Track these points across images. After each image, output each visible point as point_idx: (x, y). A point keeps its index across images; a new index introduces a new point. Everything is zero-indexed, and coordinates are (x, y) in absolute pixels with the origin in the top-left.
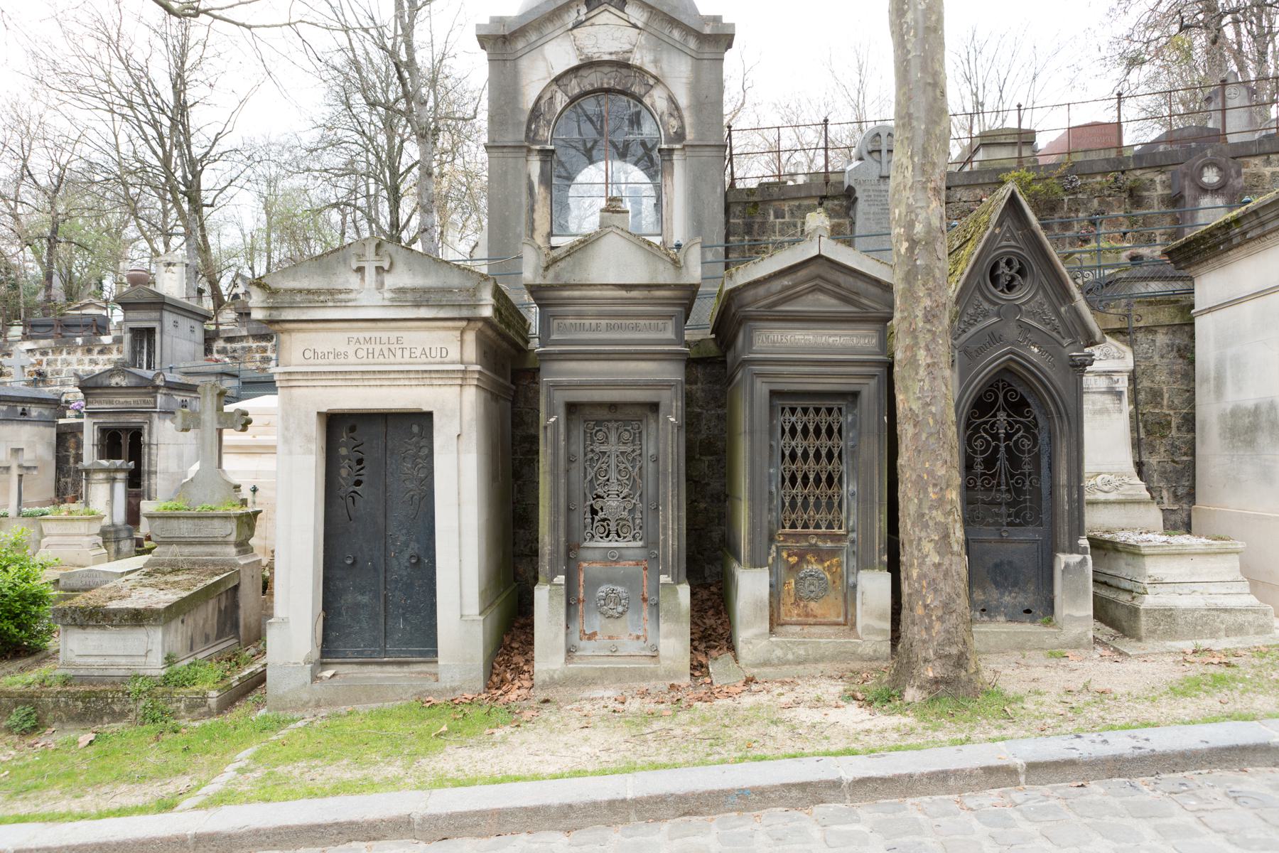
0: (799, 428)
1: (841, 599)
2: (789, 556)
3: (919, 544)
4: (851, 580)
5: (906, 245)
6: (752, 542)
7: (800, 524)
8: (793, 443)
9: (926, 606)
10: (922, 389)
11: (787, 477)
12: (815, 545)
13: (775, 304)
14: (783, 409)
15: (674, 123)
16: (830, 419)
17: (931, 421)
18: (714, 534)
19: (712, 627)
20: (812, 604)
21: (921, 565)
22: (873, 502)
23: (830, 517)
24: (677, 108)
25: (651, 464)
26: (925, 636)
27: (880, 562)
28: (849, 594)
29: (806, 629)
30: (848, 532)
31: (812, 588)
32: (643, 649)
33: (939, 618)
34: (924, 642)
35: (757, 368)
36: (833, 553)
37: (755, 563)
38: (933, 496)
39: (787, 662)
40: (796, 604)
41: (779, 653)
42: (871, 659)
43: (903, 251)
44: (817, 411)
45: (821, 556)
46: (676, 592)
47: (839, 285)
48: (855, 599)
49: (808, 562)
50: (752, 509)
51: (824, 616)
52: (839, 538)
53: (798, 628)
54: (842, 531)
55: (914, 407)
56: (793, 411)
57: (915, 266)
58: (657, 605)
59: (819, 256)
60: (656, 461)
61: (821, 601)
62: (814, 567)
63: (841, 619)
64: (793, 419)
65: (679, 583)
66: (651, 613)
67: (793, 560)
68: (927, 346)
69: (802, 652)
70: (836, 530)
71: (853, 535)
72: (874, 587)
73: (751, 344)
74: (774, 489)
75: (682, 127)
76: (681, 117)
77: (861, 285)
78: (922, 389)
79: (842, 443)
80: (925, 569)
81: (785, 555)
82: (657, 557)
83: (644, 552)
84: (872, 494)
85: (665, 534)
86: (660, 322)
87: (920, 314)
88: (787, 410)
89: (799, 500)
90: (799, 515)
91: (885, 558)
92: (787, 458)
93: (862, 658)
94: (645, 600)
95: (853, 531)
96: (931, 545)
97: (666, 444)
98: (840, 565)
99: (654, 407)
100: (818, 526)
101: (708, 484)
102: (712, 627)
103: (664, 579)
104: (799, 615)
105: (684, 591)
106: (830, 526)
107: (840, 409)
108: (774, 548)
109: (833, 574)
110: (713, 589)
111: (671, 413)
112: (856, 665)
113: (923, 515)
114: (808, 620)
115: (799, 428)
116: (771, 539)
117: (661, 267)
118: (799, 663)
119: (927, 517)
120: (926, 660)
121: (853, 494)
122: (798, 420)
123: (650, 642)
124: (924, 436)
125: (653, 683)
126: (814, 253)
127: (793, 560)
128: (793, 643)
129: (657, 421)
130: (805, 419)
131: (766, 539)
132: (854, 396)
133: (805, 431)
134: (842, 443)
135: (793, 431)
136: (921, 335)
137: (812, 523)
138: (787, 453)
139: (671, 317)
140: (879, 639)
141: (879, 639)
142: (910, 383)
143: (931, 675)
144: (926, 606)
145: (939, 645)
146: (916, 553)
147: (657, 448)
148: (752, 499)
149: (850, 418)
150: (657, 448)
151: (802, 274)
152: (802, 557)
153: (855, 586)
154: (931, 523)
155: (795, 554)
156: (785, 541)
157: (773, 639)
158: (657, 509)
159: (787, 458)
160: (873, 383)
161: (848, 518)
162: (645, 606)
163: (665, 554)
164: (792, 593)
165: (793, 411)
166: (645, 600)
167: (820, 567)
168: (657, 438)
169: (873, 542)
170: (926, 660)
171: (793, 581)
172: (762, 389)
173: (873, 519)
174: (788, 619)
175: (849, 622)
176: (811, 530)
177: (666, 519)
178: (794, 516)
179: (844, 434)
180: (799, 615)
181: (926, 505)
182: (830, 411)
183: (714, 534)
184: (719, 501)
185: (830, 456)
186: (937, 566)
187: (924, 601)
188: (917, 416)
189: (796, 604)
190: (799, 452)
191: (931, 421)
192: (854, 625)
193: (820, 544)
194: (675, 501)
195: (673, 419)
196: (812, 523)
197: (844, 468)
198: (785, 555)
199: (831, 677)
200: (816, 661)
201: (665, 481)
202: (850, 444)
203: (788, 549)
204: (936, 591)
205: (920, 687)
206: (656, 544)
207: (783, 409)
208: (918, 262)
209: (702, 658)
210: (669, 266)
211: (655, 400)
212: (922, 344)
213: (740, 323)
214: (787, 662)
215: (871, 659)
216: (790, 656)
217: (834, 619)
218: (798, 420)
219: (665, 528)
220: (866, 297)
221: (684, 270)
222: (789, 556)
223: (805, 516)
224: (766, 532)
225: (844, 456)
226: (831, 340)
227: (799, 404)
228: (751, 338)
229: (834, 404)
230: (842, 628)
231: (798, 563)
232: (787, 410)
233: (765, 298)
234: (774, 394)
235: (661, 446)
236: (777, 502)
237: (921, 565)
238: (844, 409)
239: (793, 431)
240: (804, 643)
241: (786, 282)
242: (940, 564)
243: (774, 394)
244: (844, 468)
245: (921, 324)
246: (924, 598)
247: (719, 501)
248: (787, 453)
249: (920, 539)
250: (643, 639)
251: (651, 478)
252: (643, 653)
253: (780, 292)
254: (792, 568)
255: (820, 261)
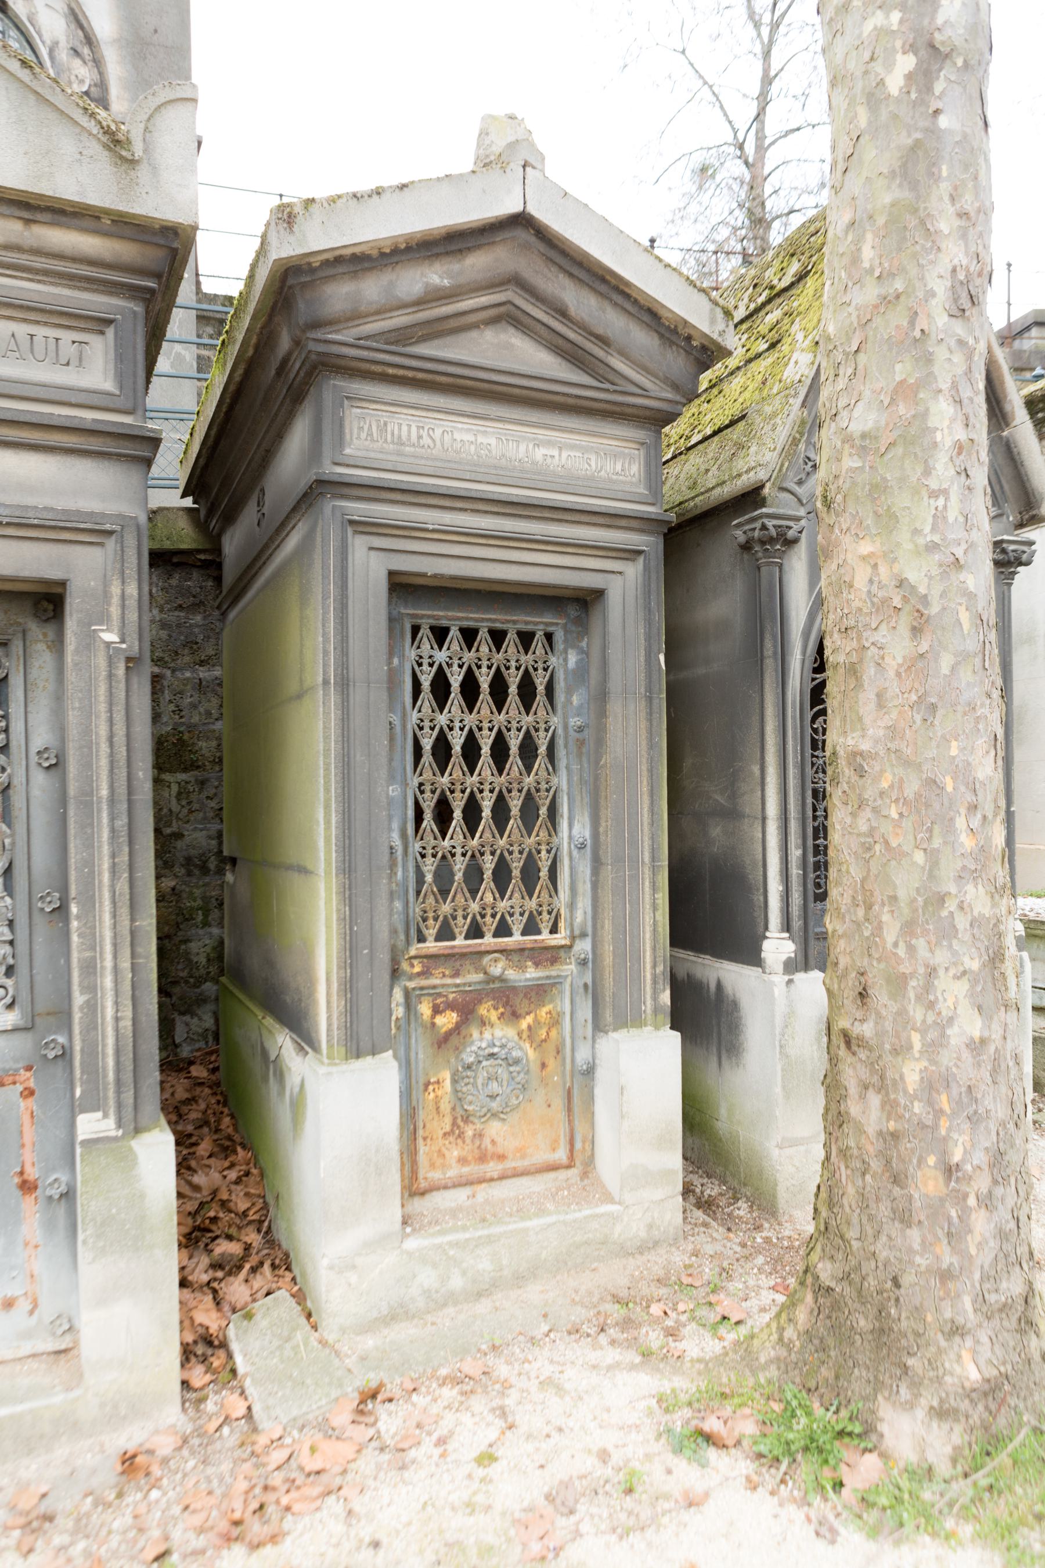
0: (456, 680)
1: (559, 1102)
2: (436, 1011)
3: (928, 987)
4: (583, 1055)
5: (907, 63)
6: (349, 987)
7: (461, 926)
8: (442, 719)
9: (950, 1171)
10: (939, 518)
11: (429, 806)
12: (501, 979)
13: (402, 336)
14: (415, 630)
15: (82, 74)
16: (527, 660)
17: (964, 617)
18: (194, 946)
19: (232, 1225)
20: (495, 1129)
21: (932, 1048)
22: (635, 862)
23: (532, 904)
24: (89, 40)
25: (39, 778)
26: (948, 1259)
27: (656, 1010)
28: (579, 1090)
29: (483, 1192)
30: (573, 938)
31: (494, 1087)
32: (27, 1335)
33: (987, 1202)
34: (946, 1276)
35: (358, 509)
36: (540, 992)
37: (358, 1045)
38: (967, 842)
39: (451, 1299)
40: (455, 1132)
41: (427, 1278)
42: (641, 1250)
43: (895, 83)
44: (498, 637)
45: (511, 1001)
46: (129, 1160)
47: (562, 313)
48: (590, 1099)
49: (483, 1023)
50: (349, 895)
51: (521, 1151)
52: (550, 955)
53: (461, 1195)
54: (560, 939)
55: (913, 576)
56: (440, 635)
57: (933, 131)
58: (68, 1196)
59: (522, 221)
60: (56, 766)
61: (514, 1118)
62: (495, 1033)
63: (561, 1155)
64: (441, 656)
65: (137, 1131)
66: (49, 1226)
67: (447, 1020)
68: (955, 386)
69: (485, 1265)
70: (545, 937)
71: (584, 946)
72: (646, 1063)
73: (340, 441)
74: (397, 842)
75: (102, 84)
76: (98, 63)
77: (612, 321)
78: (939, 518)
79: (555, 720)
80: (946, 1058)
81: (425, 1009)
82: (65, 1055)
83: (23, 1043)
84: (634, 843)
85: (91, 988)
86: (67, 336)
87: (941, 288)
88: (425, 631)
89: (459, 865)
90: (461, 906)
91: (666, 997)
92: (427, 758)
93: (625, 1252)
94: (27, 1187)
95: (583, 935)
96: (962, 988)
97: (88, 712)
98: (555, 1021)
99: (47, 601)
100: (503, 930)
101: (178, 836)
102: (232, 1225)
103: (90, 1125)
104: (462, 1161)
105: (157, 1150)
106: (532, 928)
107: (549, 637)
108: (398, 995)
109: (540, 1045)
110: (198, 1071)
111: (103, 618)
112: (616, 1275)
113: (941, 899)
114: (487, 1167)
115: (456, 680)
116: (395, 973)
117: (67, 144)
118: (480, 1295)
119: (951, 905)
120: (956, 1330)
121: (582, 847)
122: (453, 658)
123: (47, 1311)
124: (946, 662)
125: (61, 1452)
126: (512, 206)
127: (447, 1020)
128: (456, 1244)
129: (58, 645)
130: (469, 657)
131: (386, 976)
132: (582, 603)
133: (470, 690)
134: (555, 720)
135: (441, 688)
136: (941, 353)
137: (490, 924)
138: (427, 744)
139: (101, 324)
140: (658, 1194)
141: (658, 1194)
142: (901, 500)
143: (974, 1375)
144: (950, 1171)
145: (985, 1278)
146: (917, 1013)
147: (61, 729)
148: (347, 868)
149: (573, 659)
150: (61, 729)
151: (477, 263)
152: (467, 1010)
153: (590, 1072)
154: (962, 922)
155: (451, 1006)
156: (425, 973)
157: (412, 1244)
158: (61, 910)
159: (427, 758)
160: (633, 570)
161: (572, 906)
162: (30, 1209)
163: (92, 1052)
164: (445, 1106)
165: (440, 635)
166: (27, 1187)
167: (511, 1032)
168: (59, 698)
169: (638, 958)
170: (956, 1330)
171: (446, 1076)
172: (369, 566)
173: (636, 904)
174: (436, 1175)
175: (578, 1158)
176: (460, 942)
177: (92, 943)
178: (446, 908)
179: (560, 697)
180: (462, 1161)
181: (948, 869)
182: (526, 639)
183: (194, 946)
184: (204, 870)
185: (528, 750)
186: (977, 1046)
187: (944, 1154)
188: (925, 599)
189: (455, 1132)
190: (457, 741)
191: (964, 617)
192: (590, 1162)
193: (511, 974)
194: (123, 886)
195: (111, 637)
196: (490, 924)
197: (561, 780)
198: (425, 1009)
199: (574, 1331)
200: (520, 1280)
201: (88, 822)
202: (574, 721)
203: (434, 993)
204: (974, 1120)
205: (942, 1413)
206: (62, 1016)
207: (415, 630)
208: (943, 122)
209: (208, 1317)
210: (94, 148)
211: (54, 574)
212: (945, 385)
213: (297, 396)
214: (451, 1299)
215: (641, 1250)
216: (457, 1282)
217: (542, 1156)
218: (453, 658)
219: (90, 968)
220: (623, 353)
221: (143, 173)
222: (436, 1011)
223: (474, 907)
224: (384, 957)
225: (561, 753)
226: (539, 453)
227: (455, 618)
228: (341, 420)
229: (538, 622)
230: (562, 1174)
231: (457, 1028)
232: (425, 631)
233: (380, 312)
234: (401, 587)
235: (73, 717)
236: (405, 874)
237: (932, 1048)
238: (559, 636)
239: (441, 688)
240: (490, 1240)
241: (435, 275)
242: (983, 1041)
243: (401, 587)
244: (561, 780)
245: (942, 320)
246: (943, 1147)
247: (204, 870)
248: (427, 744)
249: (932, 972)
250: (23, 1306)
251: (41, 819)
252: (27, 1348)
253: (420, 303)
254: (444, 1041)
255: (523, 235)
